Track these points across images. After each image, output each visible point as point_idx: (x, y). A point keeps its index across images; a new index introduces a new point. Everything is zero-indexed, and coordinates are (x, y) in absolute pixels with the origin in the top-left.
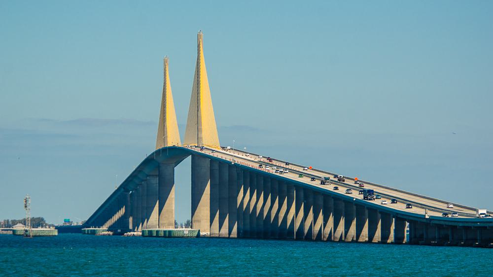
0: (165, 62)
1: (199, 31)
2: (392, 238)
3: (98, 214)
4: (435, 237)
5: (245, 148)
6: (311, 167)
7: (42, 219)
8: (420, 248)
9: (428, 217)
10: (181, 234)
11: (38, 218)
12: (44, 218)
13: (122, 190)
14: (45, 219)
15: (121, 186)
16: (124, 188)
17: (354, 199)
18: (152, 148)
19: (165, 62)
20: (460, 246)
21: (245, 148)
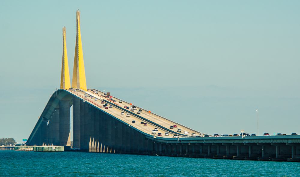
0: (64, 30)
1: (77, 10)
2: (108, 151)
3: (33, 135)
4: (192, 151)
5: (104, 90)
6: (131, 104)
7: (13, 140)
8: (291, 163)
9: (156, 138)
10: (51, 150)
11: (10, 138)
12: (14, 138)
13: (43, 119)
14: (15, 140)
15: (41, 117)
16: (44, 118)
17: (129, 126)
18: (59, 88)
19: (64, 30)
20: (215, 159)
21: (104, 90)
